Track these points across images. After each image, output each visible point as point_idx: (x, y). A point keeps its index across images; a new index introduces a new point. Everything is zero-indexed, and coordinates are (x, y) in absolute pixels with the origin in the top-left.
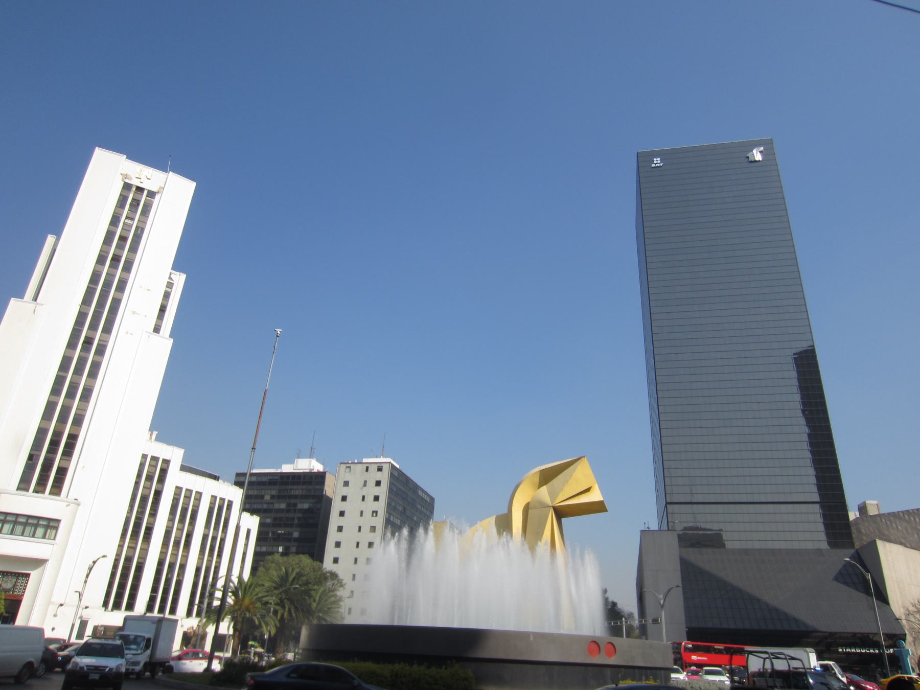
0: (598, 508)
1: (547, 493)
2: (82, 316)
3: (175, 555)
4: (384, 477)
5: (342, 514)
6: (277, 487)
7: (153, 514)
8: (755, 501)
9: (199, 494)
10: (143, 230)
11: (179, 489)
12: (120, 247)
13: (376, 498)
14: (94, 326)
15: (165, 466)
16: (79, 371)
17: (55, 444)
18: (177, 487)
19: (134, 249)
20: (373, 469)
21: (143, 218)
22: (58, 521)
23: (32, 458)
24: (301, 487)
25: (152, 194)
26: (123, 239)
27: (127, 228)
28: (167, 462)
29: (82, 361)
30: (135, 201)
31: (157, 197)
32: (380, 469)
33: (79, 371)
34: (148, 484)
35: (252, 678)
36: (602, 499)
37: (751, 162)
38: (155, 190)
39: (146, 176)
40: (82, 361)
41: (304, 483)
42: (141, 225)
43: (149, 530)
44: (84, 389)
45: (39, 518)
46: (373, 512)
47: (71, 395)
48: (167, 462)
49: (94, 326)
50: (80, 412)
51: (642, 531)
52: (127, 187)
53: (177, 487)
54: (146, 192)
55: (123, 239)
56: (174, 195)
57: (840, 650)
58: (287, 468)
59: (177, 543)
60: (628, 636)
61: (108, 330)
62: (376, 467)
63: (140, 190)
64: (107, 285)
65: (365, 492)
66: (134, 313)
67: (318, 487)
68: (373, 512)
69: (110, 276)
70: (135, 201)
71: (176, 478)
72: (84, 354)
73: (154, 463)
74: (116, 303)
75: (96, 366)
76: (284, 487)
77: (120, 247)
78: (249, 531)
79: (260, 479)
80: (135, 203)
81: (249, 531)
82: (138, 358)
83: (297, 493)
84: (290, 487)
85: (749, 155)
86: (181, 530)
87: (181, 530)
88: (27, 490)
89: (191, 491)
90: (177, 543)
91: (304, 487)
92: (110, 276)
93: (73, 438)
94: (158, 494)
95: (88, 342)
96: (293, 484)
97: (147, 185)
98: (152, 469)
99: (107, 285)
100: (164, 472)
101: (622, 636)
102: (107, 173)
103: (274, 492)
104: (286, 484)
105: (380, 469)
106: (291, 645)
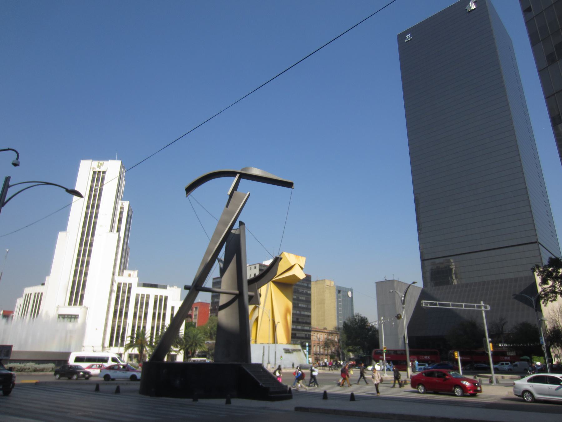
2: (83, 232)
3: (139, 323)
7: (127, 306)
8: (455, 254)
9: (148, 296)
11: (137, 296)
14: (88, 236)
16: (84, 255)
18: (137, 294)
23: (72, 292)
25: (104, 172)
28: (130, 284)
30: (98, 178)
33: (84, 255)
37: (469, 12)
40: (85, 251)
43: (126, 314)
48: (130, 284)
49: (88, 236)
51: (377, 283)
52: (94, 173)
53: (137, 294)
56: (112, 168)
57: (500, 345)
59: (140, 317)
61: (93, 236)
63: (99, 172)
70: (98, 178)
71: (137, 290)
74: (95, 223)
75: (90, 252)
82: (106, 244)
85: (467, 8)
86: (141, 312)
87: (141, 312)
89: (144, 295)
90: (140, 317)
92: (92, 213)
93: (85, 282)
94: (128, 298)
99: (91, 217)
100: (130, 289)
102: (86, 168)
106: (356, 358)
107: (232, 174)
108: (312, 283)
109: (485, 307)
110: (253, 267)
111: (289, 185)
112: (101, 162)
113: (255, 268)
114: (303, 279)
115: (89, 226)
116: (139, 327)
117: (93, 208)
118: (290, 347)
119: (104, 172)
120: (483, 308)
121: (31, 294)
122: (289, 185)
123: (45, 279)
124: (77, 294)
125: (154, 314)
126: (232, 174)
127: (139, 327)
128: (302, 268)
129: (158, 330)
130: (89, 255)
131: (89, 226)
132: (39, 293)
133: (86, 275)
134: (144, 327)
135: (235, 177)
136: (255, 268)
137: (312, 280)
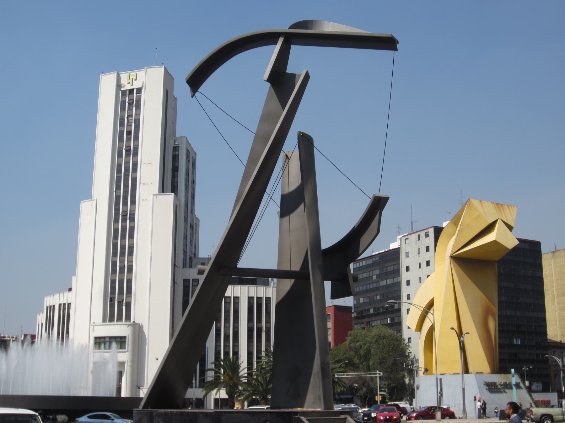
1: (310, 397)
3: (227, 346)
10: (139, 120)
12: (129, 140)
14: (125, 203)
17: (121, 288)
19: (137, 138)
22: (125, 337)
25: (139, 90)
26: (129, 133)
27: (129, 125)
30: (129, 100)
31: (143, 91)
33: (123, 237)
34: (113, 296)
35: (338, 375)
38: (140, 86)
45: (104, 338)
47: (123, 254)
49: (125, 203)
50: (130, 264)
54: (135, 91)
55: (129, 133)
59: (227, 337)
61: (133, 202)
63: (131, 91)
64: (127, 170)
66: (144, 184)
69: (127, 163)
70: (129, 100)
72: (124, 224)
74: (134, 180)
77: (129, 140)
78: (42, 324)
80: (131, 104)
81: (42, 324)
89: (261, 298)
92: (127, 163)
93: (130, 281)
97: (136, 85)
99: (127, 170)
103: (377, 272)
107: (267, 38)
108: (544, 257)
109: (379, 374)
110: (423, 234)
111: (388, 43)
112: (133, 73)
113: (427, 236)
114: (515, 248)
115: (126, 186)
116: (227, 353)
117: (128, 155)
118: (498, 379)
119: (139, 90)
120: (378, 375)
121: (54, 306)
122: (388, 43)
123: (71, 282)
124: (118, 302)
125: (250, 331)
126: (267, 38)
127: (227, 353)
128: (510, 228)
129: (259, 358)
130: (132, 236)
131: (126, 186)
132: (51, 307)
133: (130, 270)
134: (236, 353)
135: (276, 43)
136: (427, 236)
137: (543, 250)
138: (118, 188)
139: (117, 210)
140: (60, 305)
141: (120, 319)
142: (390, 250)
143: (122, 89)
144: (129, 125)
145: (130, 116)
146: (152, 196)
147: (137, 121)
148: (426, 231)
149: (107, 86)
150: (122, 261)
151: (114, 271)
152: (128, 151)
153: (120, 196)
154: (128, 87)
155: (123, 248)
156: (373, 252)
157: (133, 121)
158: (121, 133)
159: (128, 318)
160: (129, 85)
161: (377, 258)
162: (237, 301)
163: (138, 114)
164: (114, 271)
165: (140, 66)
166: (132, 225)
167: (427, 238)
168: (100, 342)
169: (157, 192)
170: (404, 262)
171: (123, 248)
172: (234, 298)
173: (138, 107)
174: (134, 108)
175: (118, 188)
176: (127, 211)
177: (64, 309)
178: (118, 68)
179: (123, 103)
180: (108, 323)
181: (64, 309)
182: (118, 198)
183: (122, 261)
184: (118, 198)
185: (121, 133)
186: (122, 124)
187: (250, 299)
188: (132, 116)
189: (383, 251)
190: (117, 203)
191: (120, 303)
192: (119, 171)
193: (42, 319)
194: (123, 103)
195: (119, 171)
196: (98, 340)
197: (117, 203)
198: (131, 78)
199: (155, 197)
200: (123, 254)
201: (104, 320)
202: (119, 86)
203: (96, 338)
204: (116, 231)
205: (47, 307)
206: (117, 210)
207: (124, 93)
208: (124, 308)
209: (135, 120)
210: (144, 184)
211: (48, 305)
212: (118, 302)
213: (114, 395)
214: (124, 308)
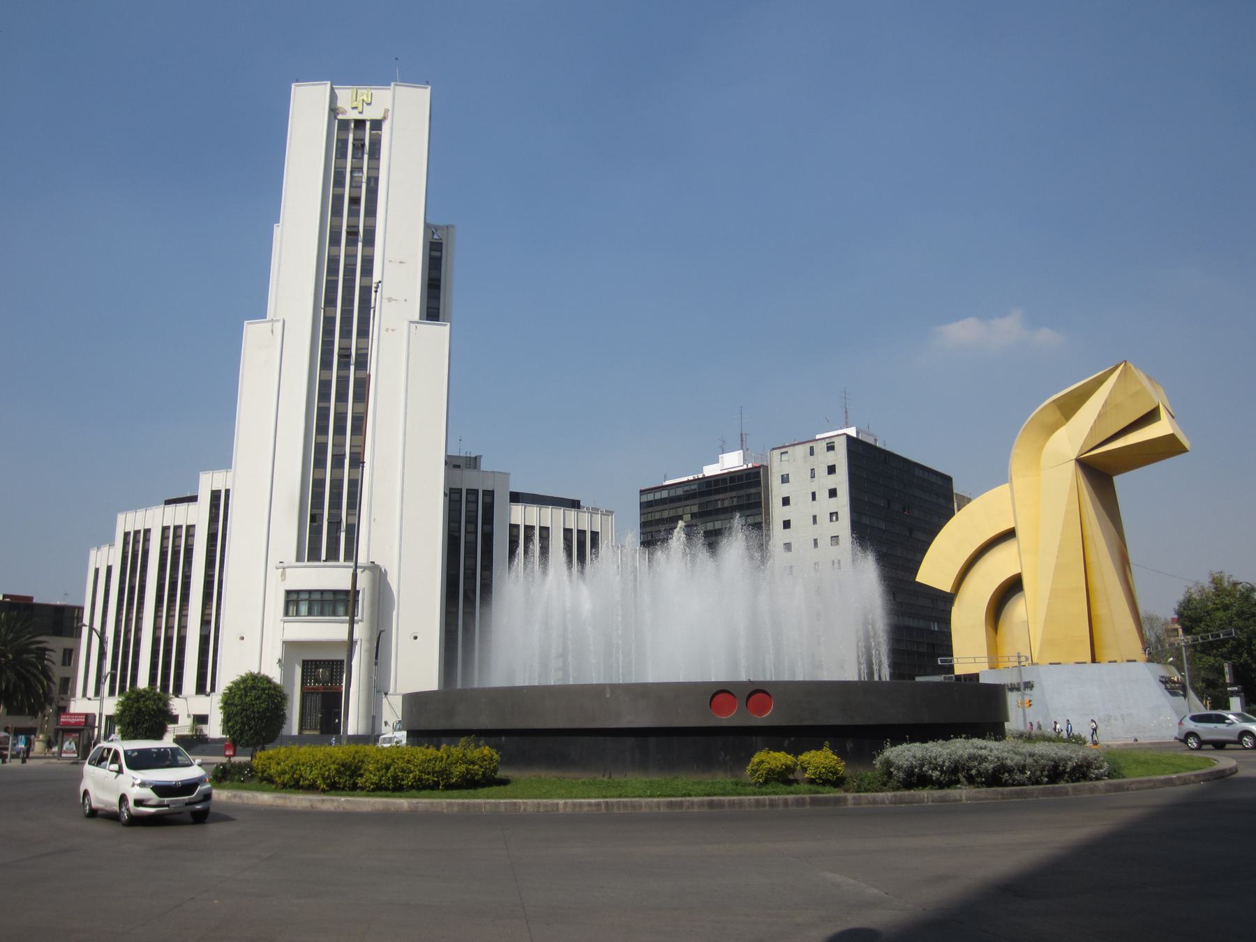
0: (1168, 447)
4: (840, 458)
5: (787, 524)
6: (697, 501)
10: (376, 179)
12: (354, 213)
13: (833, 493)
14: (346, 333)
15: (488, 499)
19: (371, 212)
20: (820, 447)
21: (373, 163)
24: (728, 495)
25: (377, 125)
26: (355, 201)
27: (355, 186)
29: (343, 382)
30: (355, 142)
31: (386, 126)
32: (831, 448)
33: (341, 397)
34: (471, 527)
36: (1171, 432)
38: (379, 117)
39: (360, 102)
41: (732, 489)
42: (373, 174)
44: (353, 418)
46: (831, 514)
47: (340, 430)
49: (346, 333)
54: (368, 124)
55: (355, 201)
58: (710, 470)
60: (116, 754)
61: (364, 332)
62: (824, 444)
63: (360, 124)
64: (350, 271)
65: (814, 486)
66: (390, 300)
67: (753, 491)
68: (831, 514)
69: (351, 257)
70: (355, 142)
72: (343, 373)
73: (472, 498)
74: (366, 292)
76: (706, 499)
77: (354, 213)
78: (109, 569)
79: (673, 493)
80: (359, 146)
81: (109, 569)
83: (727, 504)
84: (713, 498)
88: (337, 559)
91: (734, 494)
92: (351, 257)
95: (345, 356)
96: (717, 492)
97: (369, 114)
98: (472, 506)
99: (350, 271)
101: (125, 752)
103: (695, 509)
104: (709, 493)
105: (831, 448)
115: (348, 300)
119: (377, 125)
121: (147, 531)
124: (329, 519)
131: (348, 300)
138: (330, 301)
139: (328, 345)
140: (165, 529)
141: (333, 555)
142: (704, 478)
143: (340, 117)
144: (355, 186)
145: (357, 169)
146: (406, 324)
147: (373, 183)
148: (811, 444)
149: (309, 111)
150: (339, 445)
151: (320, 463)
152: (353, 233)
153: (335, 318)
154: (353, 115)
155: (340, 418)
156: (666, 479)
157: (364, 179)
158: (338, 199)
159: (351, 554)
160: (356, 111)
161: (695, 487)
162: (545, 534)
163: (374, 168)
164: (320, 463)
165: (383, 80)
166: (361, 374)
167: (831, 452)
168: (293, 599)
169: (417, 318)
170: (777, 490)
171: (340, 418)
172: (526, 527)
173: (375, 154)
174: (366, 157)
175: (330, 301)
176: (350, 349)
177: (136, 541)
178: (342, 75)
179: (342, 144)
180: (306, 563)
181: (136, 541)
182: (329, 321)
183: (339, 445)
184: (329, 321)
185: (338, 199)
186: (339, 182)
187: (568, 532)
188: (361, 169)
189: (691, 478)
190: (329, 332)
191: (335, 524)
192: (333, 270)
193: (109, 557)
194: (342, 144)
195: (333, 270)
196: (294, 597)
197: (329, 332)
198: (360, 98)
199: (413, 326)
200: (340, 430)
201: (299, 558)
202: (333, 110)
203: (288, 593)
204: (325, 385)
205: (127, 534)
206: (328, 345)
207: (344, 125)
208: (343, 535)
209: (369, 179)
210: (390, 300)
211: (130, 528)
212: (329, 519)
213: (865, 678)
214: (343, 535)
